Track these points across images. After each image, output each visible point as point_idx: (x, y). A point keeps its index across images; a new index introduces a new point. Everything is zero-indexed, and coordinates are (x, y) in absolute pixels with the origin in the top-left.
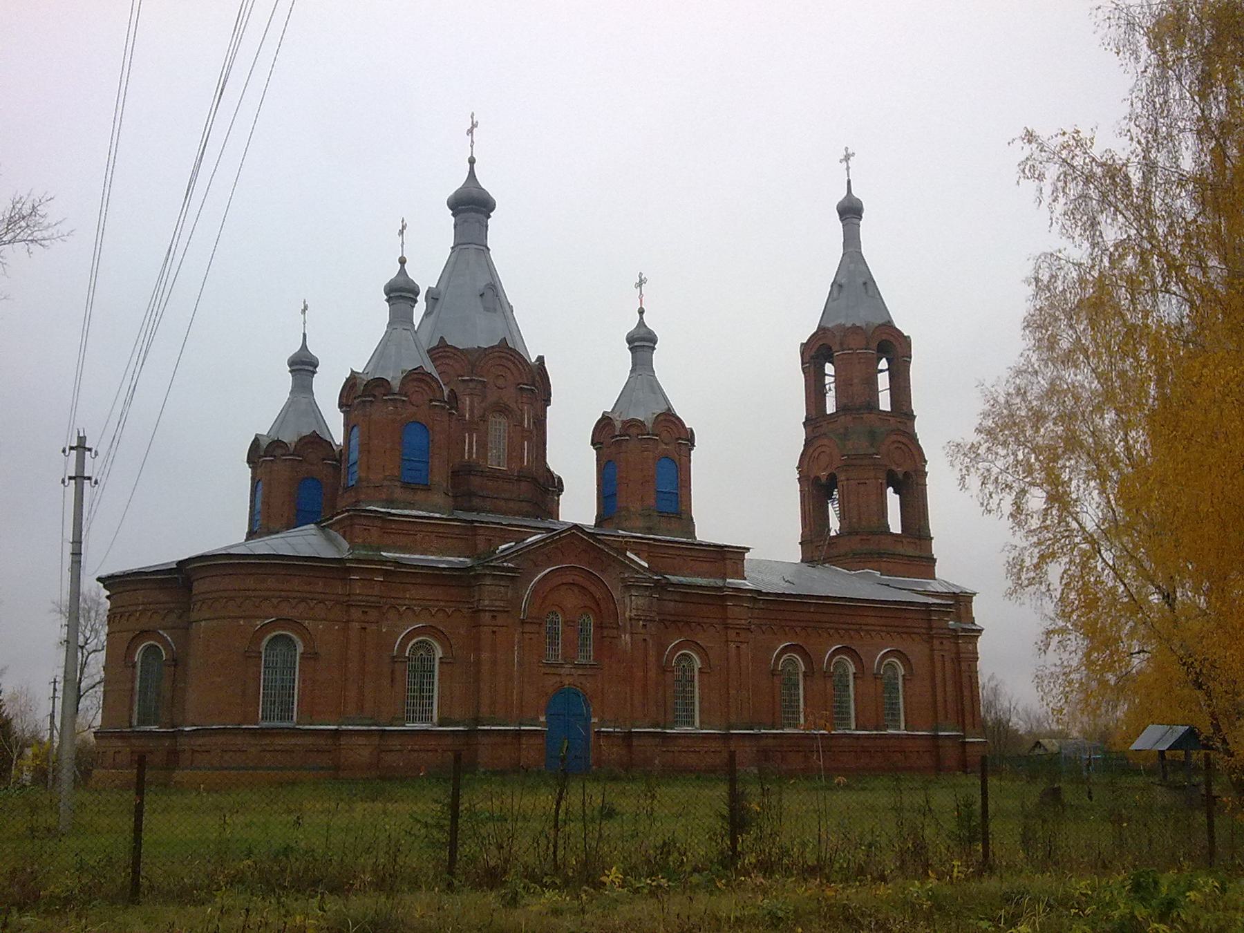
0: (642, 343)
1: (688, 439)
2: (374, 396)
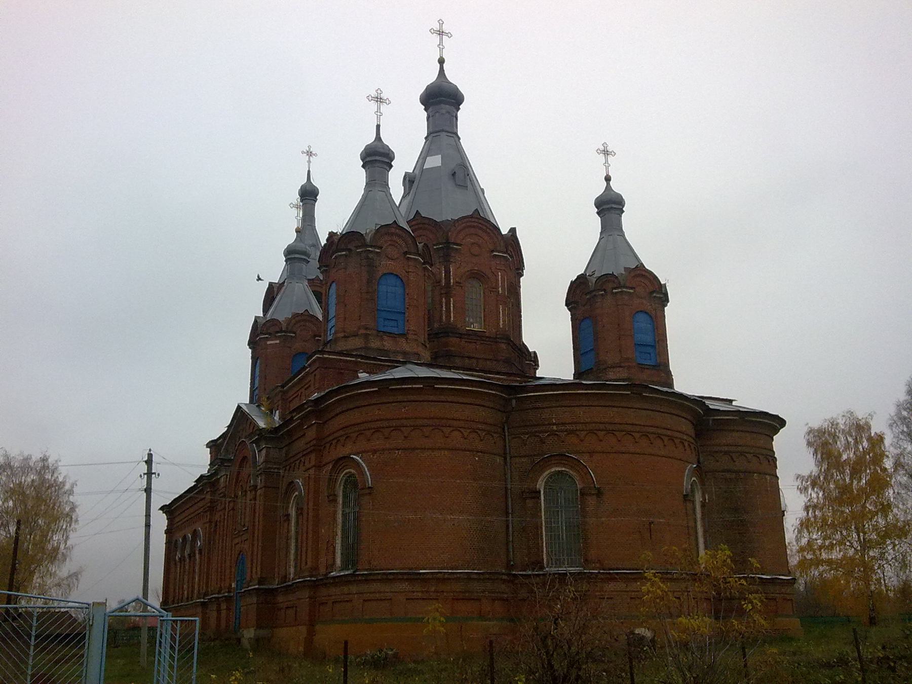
0: (610, 206)
1: (657, 294)
2: (350, 250)
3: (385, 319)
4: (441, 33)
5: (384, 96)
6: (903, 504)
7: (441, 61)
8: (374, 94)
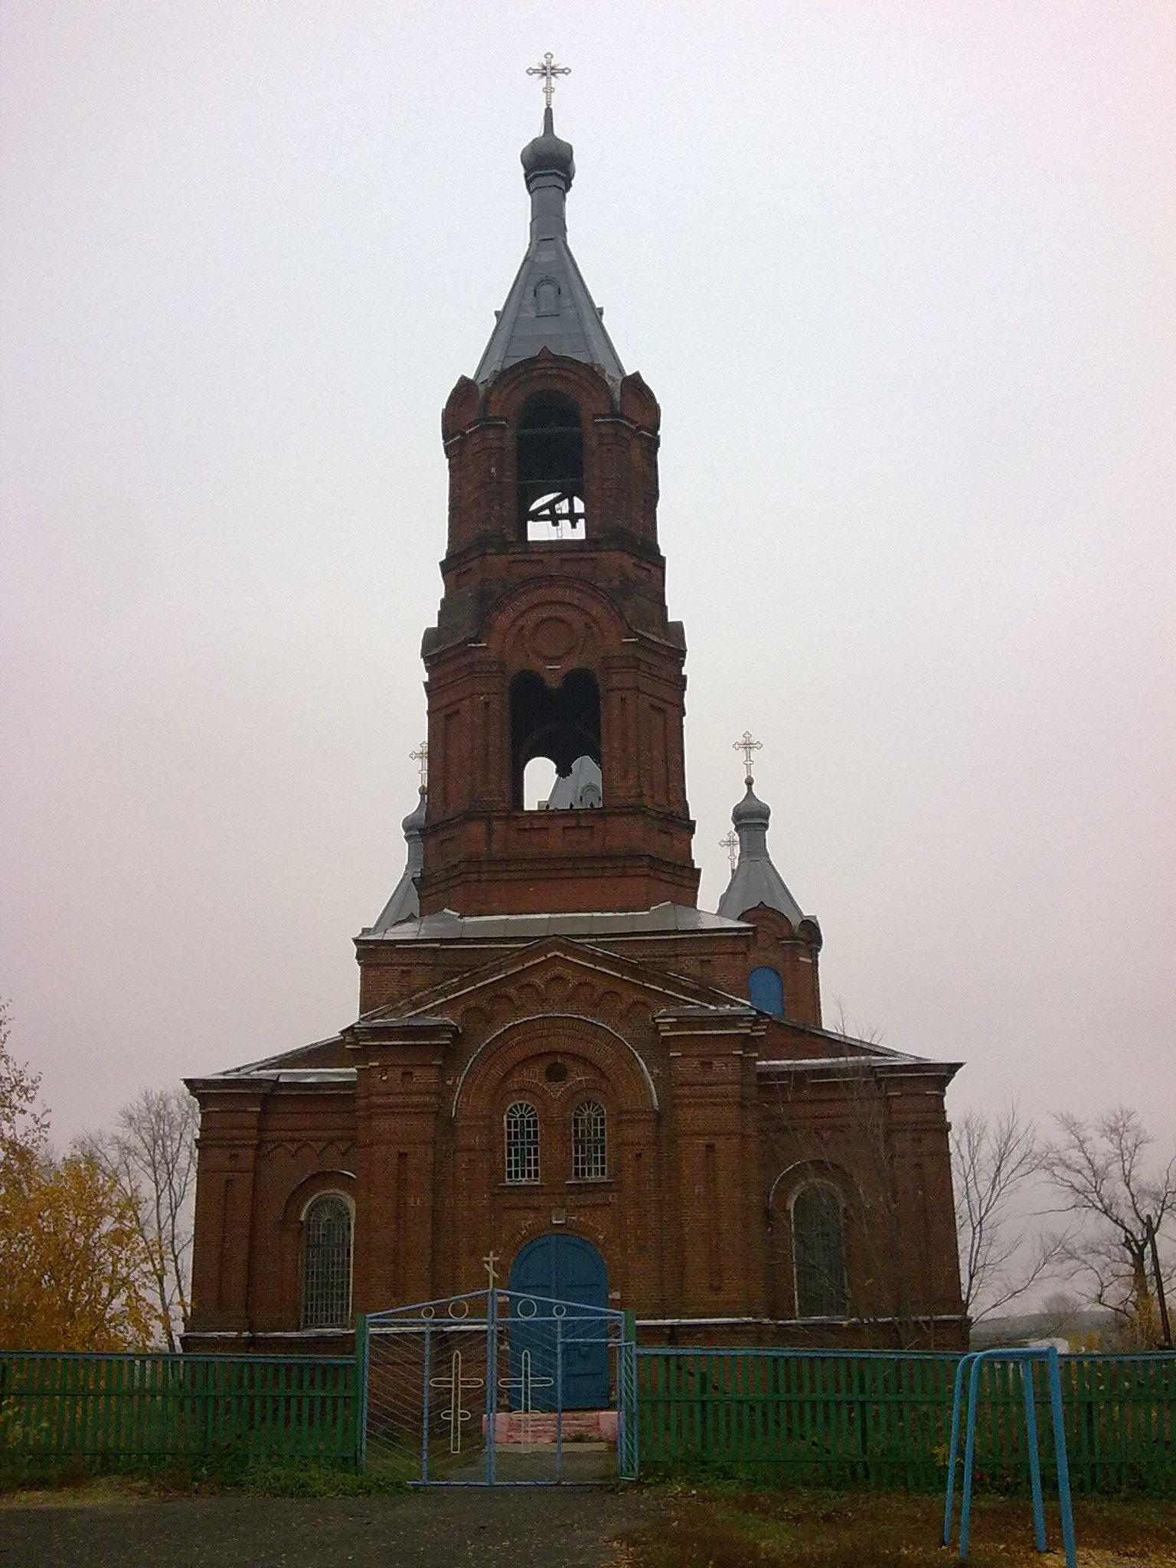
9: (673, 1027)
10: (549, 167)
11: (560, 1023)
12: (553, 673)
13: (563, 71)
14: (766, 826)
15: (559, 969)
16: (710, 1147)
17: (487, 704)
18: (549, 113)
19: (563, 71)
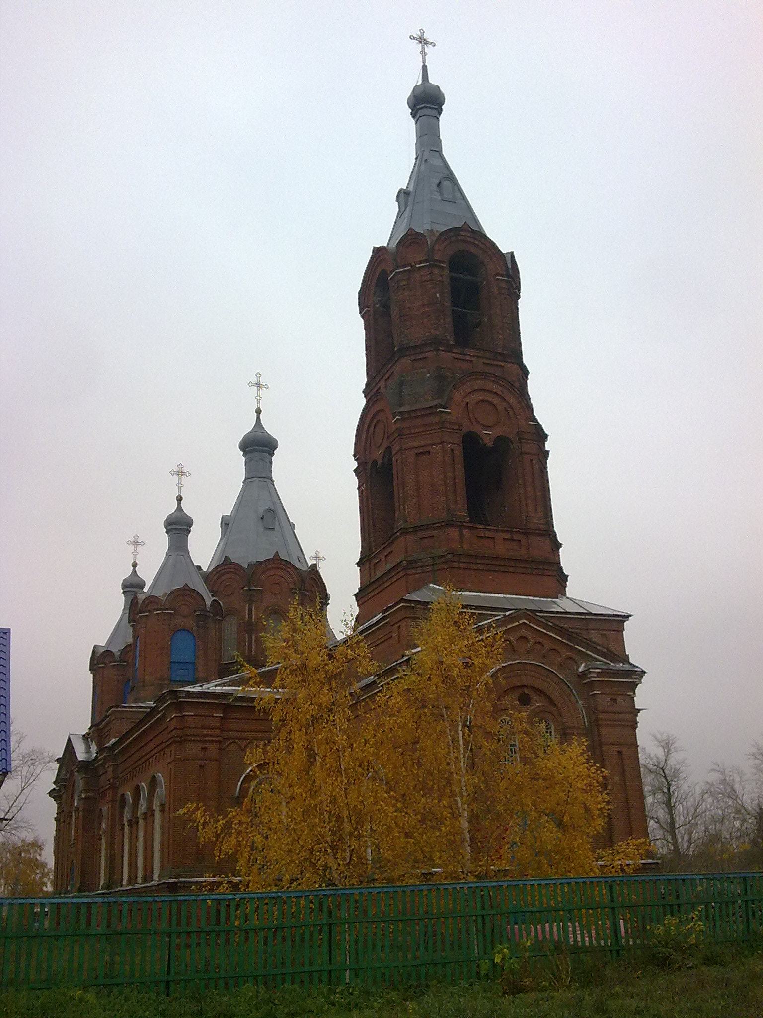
3: (89, 923)
4: (258, 385)
5: (185, 470)
6: (581, 1000)
7: (258, 411)
8: (133, 540)
9: (599, 674)
10: (426, 103)
11: (528, 667)
12: (488, 436)
13: (414, 38)
14: (189, 531)
15: (523, 632)
16: (620, 752)
17: (452, 450)
18: (425, 68)
19: (414, 38)
